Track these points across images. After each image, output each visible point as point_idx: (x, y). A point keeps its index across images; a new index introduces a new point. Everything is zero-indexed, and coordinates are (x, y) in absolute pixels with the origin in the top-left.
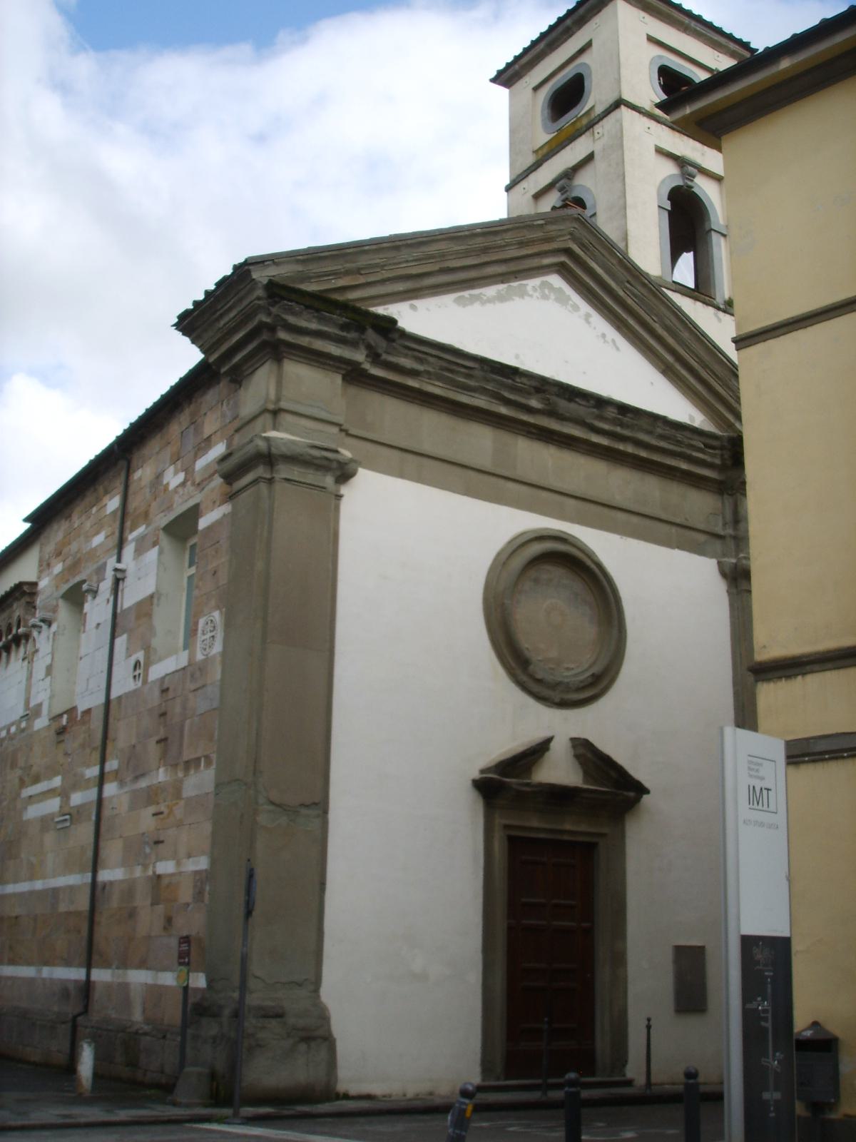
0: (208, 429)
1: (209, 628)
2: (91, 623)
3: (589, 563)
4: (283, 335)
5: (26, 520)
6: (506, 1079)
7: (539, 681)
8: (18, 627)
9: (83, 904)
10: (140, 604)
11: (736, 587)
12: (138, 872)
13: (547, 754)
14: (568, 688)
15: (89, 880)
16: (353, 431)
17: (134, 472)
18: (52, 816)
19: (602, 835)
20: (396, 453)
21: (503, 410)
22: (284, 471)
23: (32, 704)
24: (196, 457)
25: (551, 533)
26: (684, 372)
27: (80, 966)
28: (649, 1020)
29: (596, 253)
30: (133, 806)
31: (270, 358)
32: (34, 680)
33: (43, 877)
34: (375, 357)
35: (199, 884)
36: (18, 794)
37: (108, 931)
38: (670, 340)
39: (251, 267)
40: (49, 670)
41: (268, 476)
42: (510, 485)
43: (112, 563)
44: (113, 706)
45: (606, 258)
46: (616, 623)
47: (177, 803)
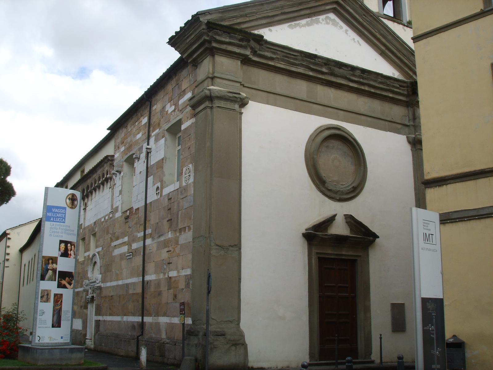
2: (138, 170)
3: (350, 139)
4: (214, 45)
5: (108, 129)
7: (330, 190)
8: (107, 174)
9: (139, 290)
11: (415, 148)
14: (342, 193)
18: (124, 253)
19: (359, 256)
20: (265, 94)
21: (311, 73)
22: (217, 103)
25: (334, 126)
26: (390, 54)
28: (381, 335)
30: (158, 248)
34: (254, 53)
35: (187, 280)
37: (150, 301)
38: (383, 40)
40: (121, 192)
42: (315, 106)
43: (145, 145)
46: (362, 164)
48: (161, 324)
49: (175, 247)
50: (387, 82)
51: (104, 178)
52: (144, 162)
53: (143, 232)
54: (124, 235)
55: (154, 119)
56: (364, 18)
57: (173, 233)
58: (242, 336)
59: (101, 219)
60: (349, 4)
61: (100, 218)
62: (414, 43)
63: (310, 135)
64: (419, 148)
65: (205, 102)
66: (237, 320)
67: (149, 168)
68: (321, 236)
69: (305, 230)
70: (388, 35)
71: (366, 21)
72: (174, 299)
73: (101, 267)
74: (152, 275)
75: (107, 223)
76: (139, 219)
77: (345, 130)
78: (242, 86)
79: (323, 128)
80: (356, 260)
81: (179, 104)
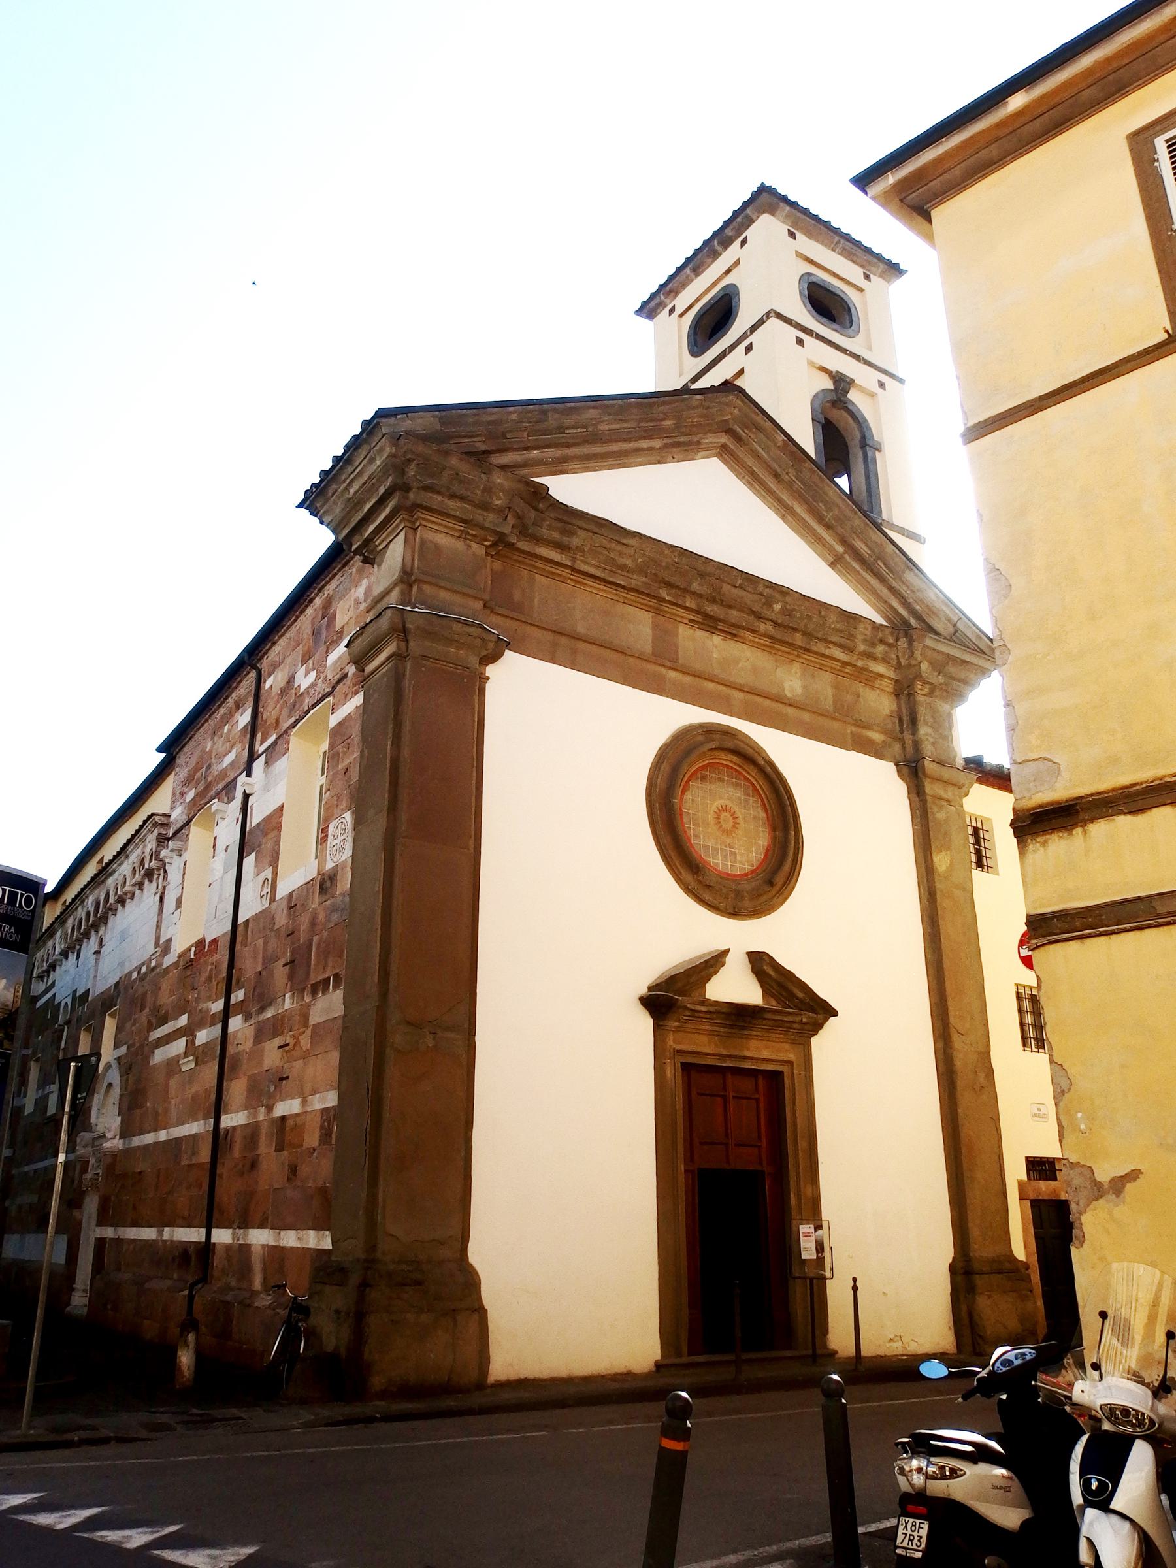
5: (159, 750)
6: (690, 1354)
8: (151, 861)
9: (205, 1155)
10: (268, 819)
17: (265, 682)
24: (327, 652)
28: (855, 1280)
33: (165, 1127)
35: (326, 1124)
36: (147, 1038)
37: (229, 1189)
44: (240, 931)
55: (270, 712)
59: (130, 974)
69: (647, 990)
72: (289, 1179)
73: (121, 1096)
74: (240, 1114)
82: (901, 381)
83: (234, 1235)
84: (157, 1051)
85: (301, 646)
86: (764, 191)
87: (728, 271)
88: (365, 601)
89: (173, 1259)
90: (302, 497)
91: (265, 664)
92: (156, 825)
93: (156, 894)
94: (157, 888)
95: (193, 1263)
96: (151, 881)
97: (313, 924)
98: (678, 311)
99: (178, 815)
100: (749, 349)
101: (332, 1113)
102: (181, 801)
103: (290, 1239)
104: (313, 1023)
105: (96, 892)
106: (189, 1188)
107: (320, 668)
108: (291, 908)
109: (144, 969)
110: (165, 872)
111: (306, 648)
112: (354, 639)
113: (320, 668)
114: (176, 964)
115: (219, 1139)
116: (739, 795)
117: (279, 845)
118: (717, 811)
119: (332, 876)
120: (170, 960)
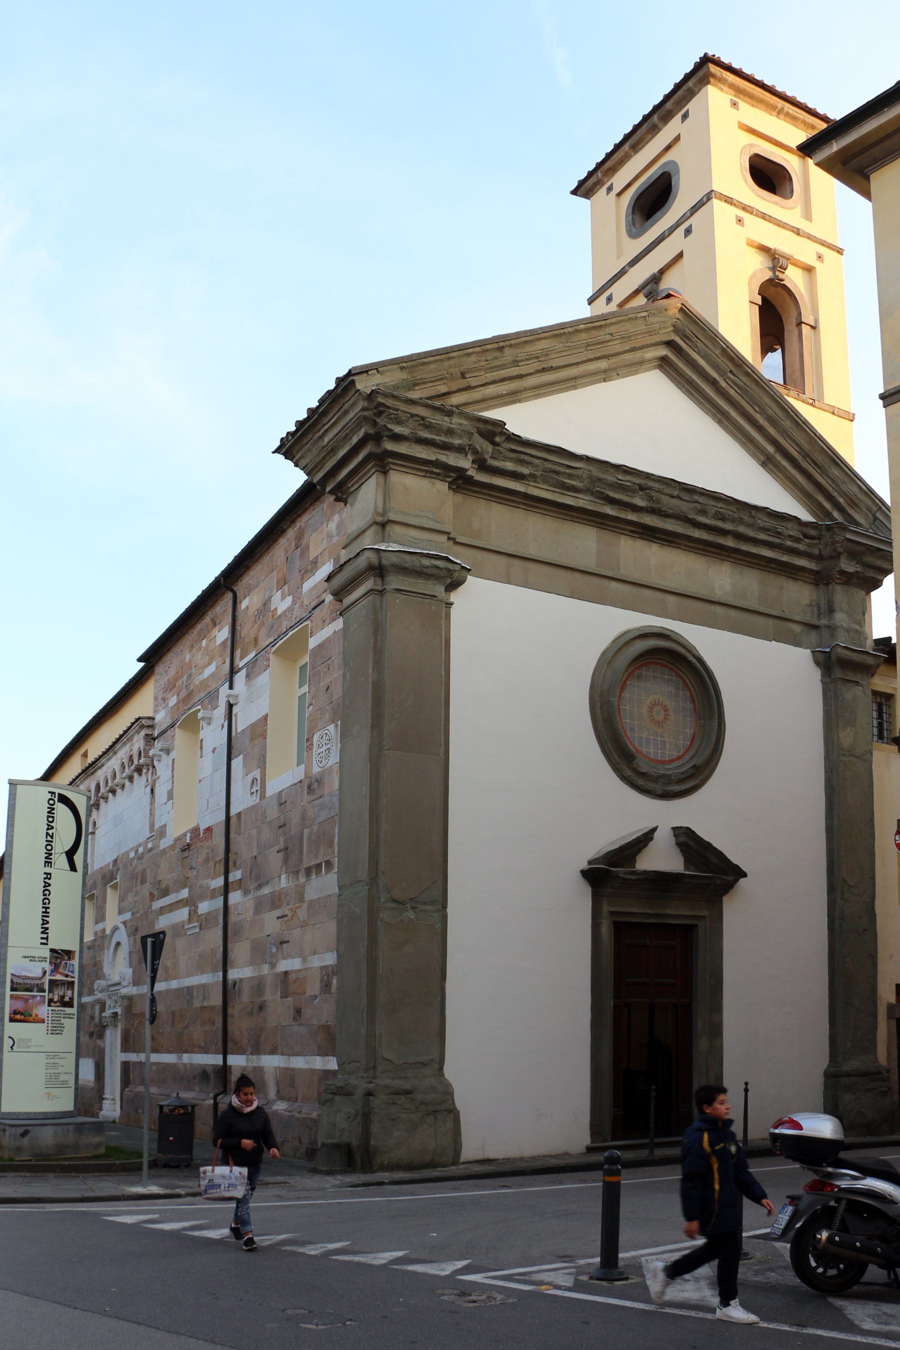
0: (313, 553)
1: (324, 740)
2: (208, 747)
3: (691, 658)
4: (389, 446)
5: (139, 660)
6: (612, 1140)
7: (643, 775)
8: (140, 758)
9: (216, 1000)
10: (253, 726)
11: (830, 676)
12: (266, 969)
13: (651, 843)
14: (668, 779)
15: (221, 979)
16: (460, 539)
17: (241, 602)
18: (182, 925)
20: (503, 560)
21: (609, 510)
22: (394, 582)
23: (156, 826)
24: (303, 580)
25: (655, 630)
26: (784, 463)
27: (216, 1053)
28: (746, 1084)
29: (700, 344)
30: (259, 908)
31: (376, 471)
32: (157, 804)
33: (176, 977)
34: (482, 465)
35: (325, 978)
36: (150, 907)
37: (240, 1025)
38: (772, 431)
39: (355, 378)
40: (170, 795)
41: (380, 588)
42: (614, 584)
43: (224, 691)
44: (233, 822)
45: (709, 349)
46: (716, 716)
47: (301, 906)
48: (266, 1070)
49: (297, 908)
50: (776, 528)
51: (132, 765)
52: (222, 728)
53: (222, 878)
54: (184, 883)
55: (246, 631)
56: (730, 379)
57: (290, 879)
58: (449, 1094)
59: (127, 853)
60: (697, 346)
61: (126, 852)
62: (884, 407)
63: (601, 652)
64: (838, 676)
65: (366, 580)
66: (437, 1059)
67: (233, 740)
68: (621, 875)
69: (587, 863)
70: (784, 419)
71: (734, 387)
72: (294, 1018)
73: (130, 953)
74: (246, 969)
75: (142, 860)
76: (212, 850)
77: (681, 638)
78: (452, 542)
79: (631, 636)
80: (692, 928)
81: (302, 591)
82: (840, 251)
83: (248, 1061)
84: (160, 918)
85: (275, 572)
86: (706, 60)
87: (668, 148)
88: (338, 534)
89: (194, 1078)
90: (278, 444)
91: (240, 588)
92: (142, 727)
93: (146, 786)
94: (147, 781)
95: (212, 1080)
96: (140, 774)
97: (303, 818)
98: (617, 189)
99: (162, 718)
100: (688, 231)
101: (331, 969)
102: (163, 706)
103: (299, 1063)
104: (308, 899)
105: (87, 782)
106: (203, 1024)
107: (296, 592)
108: (281, 804)
109: (141, 850)
110: (154, 767)
111: (281, 575)
112: (334, 575)
113: (296, 592)
114: (173, 847)
115: (228, 989)
116: (670, 690)
117: (265, 750)
118: (651, 705)
119: (319, 778)
120: (165, 843)
